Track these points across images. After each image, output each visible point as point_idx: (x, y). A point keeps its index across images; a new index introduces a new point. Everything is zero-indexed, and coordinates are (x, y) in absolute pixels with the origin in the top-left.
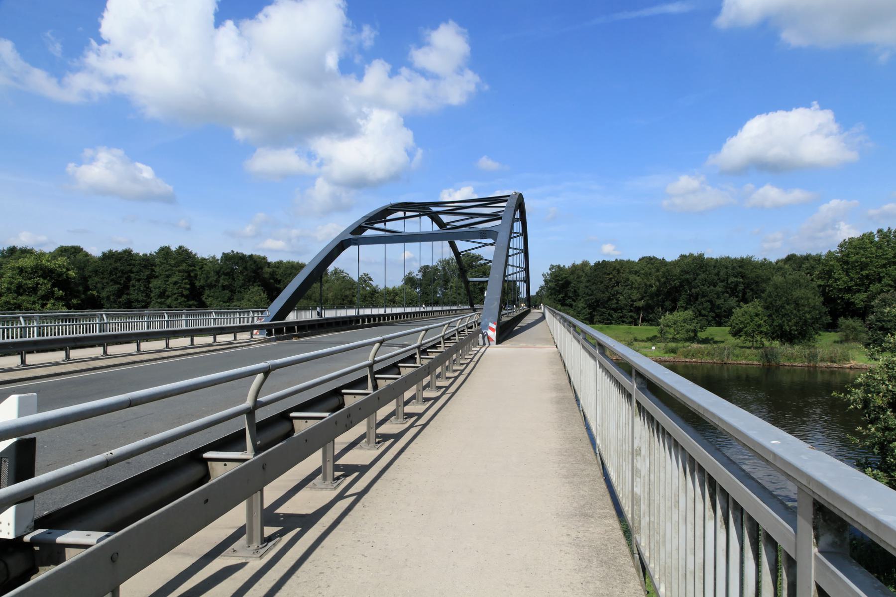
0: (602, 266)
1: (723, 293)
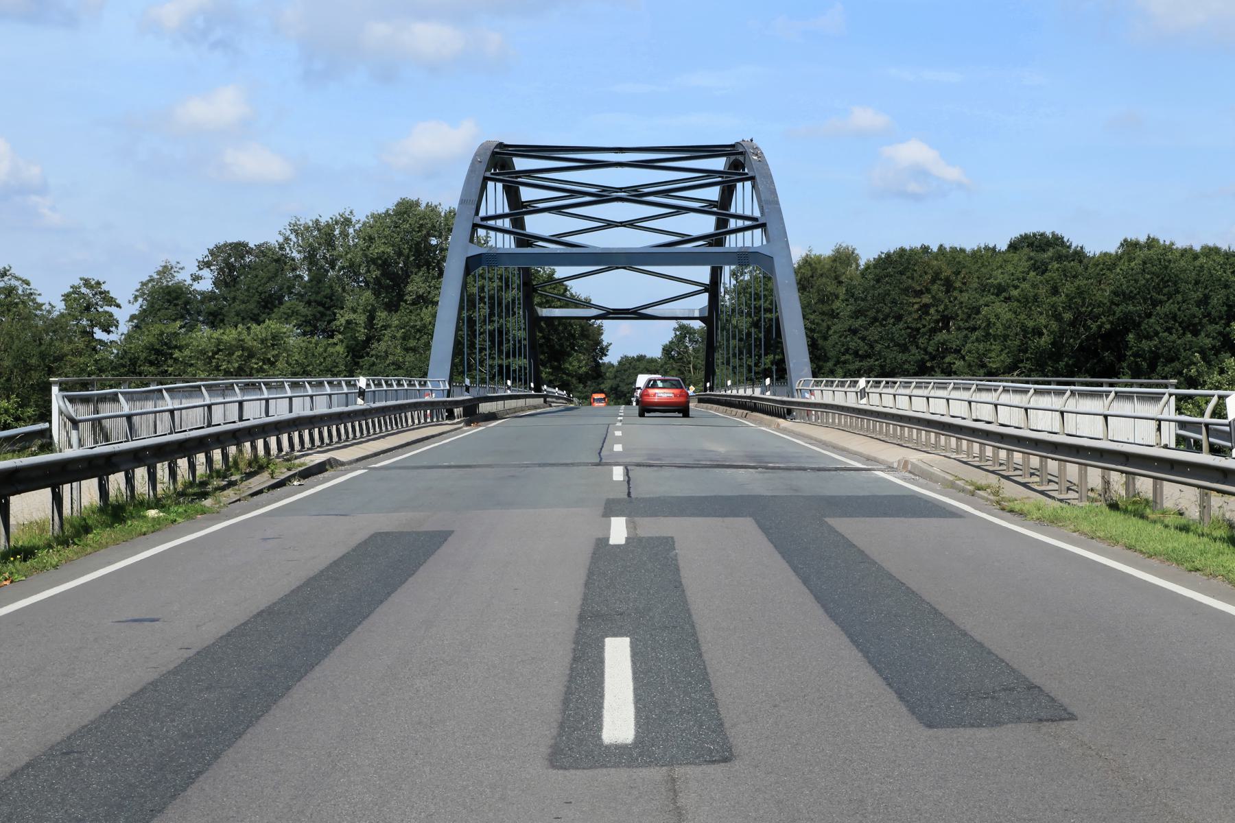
0: (898, 265)
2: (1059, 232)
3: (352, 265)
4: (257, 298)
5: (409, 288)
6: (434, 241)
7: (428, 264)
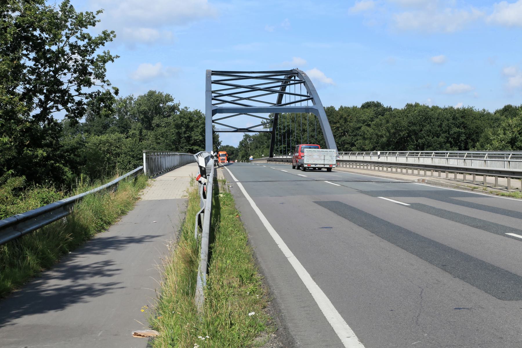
1: (445, 143)
2: (379, 101)
3: (134, 114)
4: (101, 125)
5: (154, 122)
6: (161, 105)
7: (160, 113)
